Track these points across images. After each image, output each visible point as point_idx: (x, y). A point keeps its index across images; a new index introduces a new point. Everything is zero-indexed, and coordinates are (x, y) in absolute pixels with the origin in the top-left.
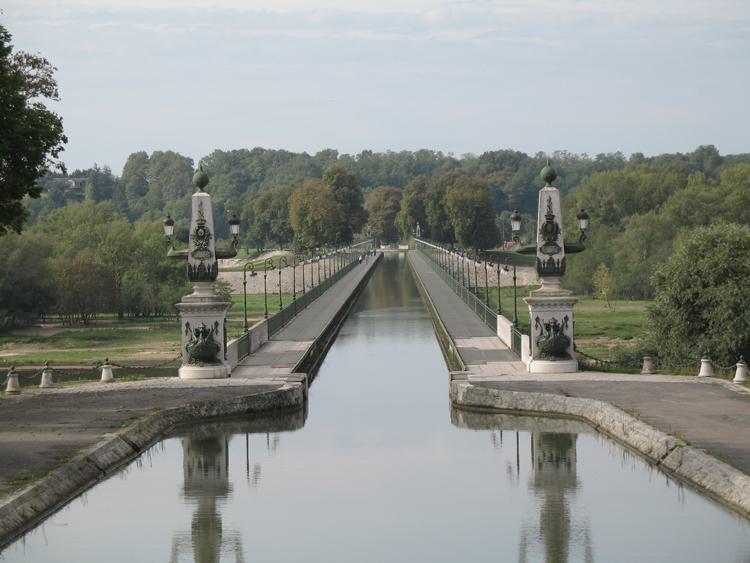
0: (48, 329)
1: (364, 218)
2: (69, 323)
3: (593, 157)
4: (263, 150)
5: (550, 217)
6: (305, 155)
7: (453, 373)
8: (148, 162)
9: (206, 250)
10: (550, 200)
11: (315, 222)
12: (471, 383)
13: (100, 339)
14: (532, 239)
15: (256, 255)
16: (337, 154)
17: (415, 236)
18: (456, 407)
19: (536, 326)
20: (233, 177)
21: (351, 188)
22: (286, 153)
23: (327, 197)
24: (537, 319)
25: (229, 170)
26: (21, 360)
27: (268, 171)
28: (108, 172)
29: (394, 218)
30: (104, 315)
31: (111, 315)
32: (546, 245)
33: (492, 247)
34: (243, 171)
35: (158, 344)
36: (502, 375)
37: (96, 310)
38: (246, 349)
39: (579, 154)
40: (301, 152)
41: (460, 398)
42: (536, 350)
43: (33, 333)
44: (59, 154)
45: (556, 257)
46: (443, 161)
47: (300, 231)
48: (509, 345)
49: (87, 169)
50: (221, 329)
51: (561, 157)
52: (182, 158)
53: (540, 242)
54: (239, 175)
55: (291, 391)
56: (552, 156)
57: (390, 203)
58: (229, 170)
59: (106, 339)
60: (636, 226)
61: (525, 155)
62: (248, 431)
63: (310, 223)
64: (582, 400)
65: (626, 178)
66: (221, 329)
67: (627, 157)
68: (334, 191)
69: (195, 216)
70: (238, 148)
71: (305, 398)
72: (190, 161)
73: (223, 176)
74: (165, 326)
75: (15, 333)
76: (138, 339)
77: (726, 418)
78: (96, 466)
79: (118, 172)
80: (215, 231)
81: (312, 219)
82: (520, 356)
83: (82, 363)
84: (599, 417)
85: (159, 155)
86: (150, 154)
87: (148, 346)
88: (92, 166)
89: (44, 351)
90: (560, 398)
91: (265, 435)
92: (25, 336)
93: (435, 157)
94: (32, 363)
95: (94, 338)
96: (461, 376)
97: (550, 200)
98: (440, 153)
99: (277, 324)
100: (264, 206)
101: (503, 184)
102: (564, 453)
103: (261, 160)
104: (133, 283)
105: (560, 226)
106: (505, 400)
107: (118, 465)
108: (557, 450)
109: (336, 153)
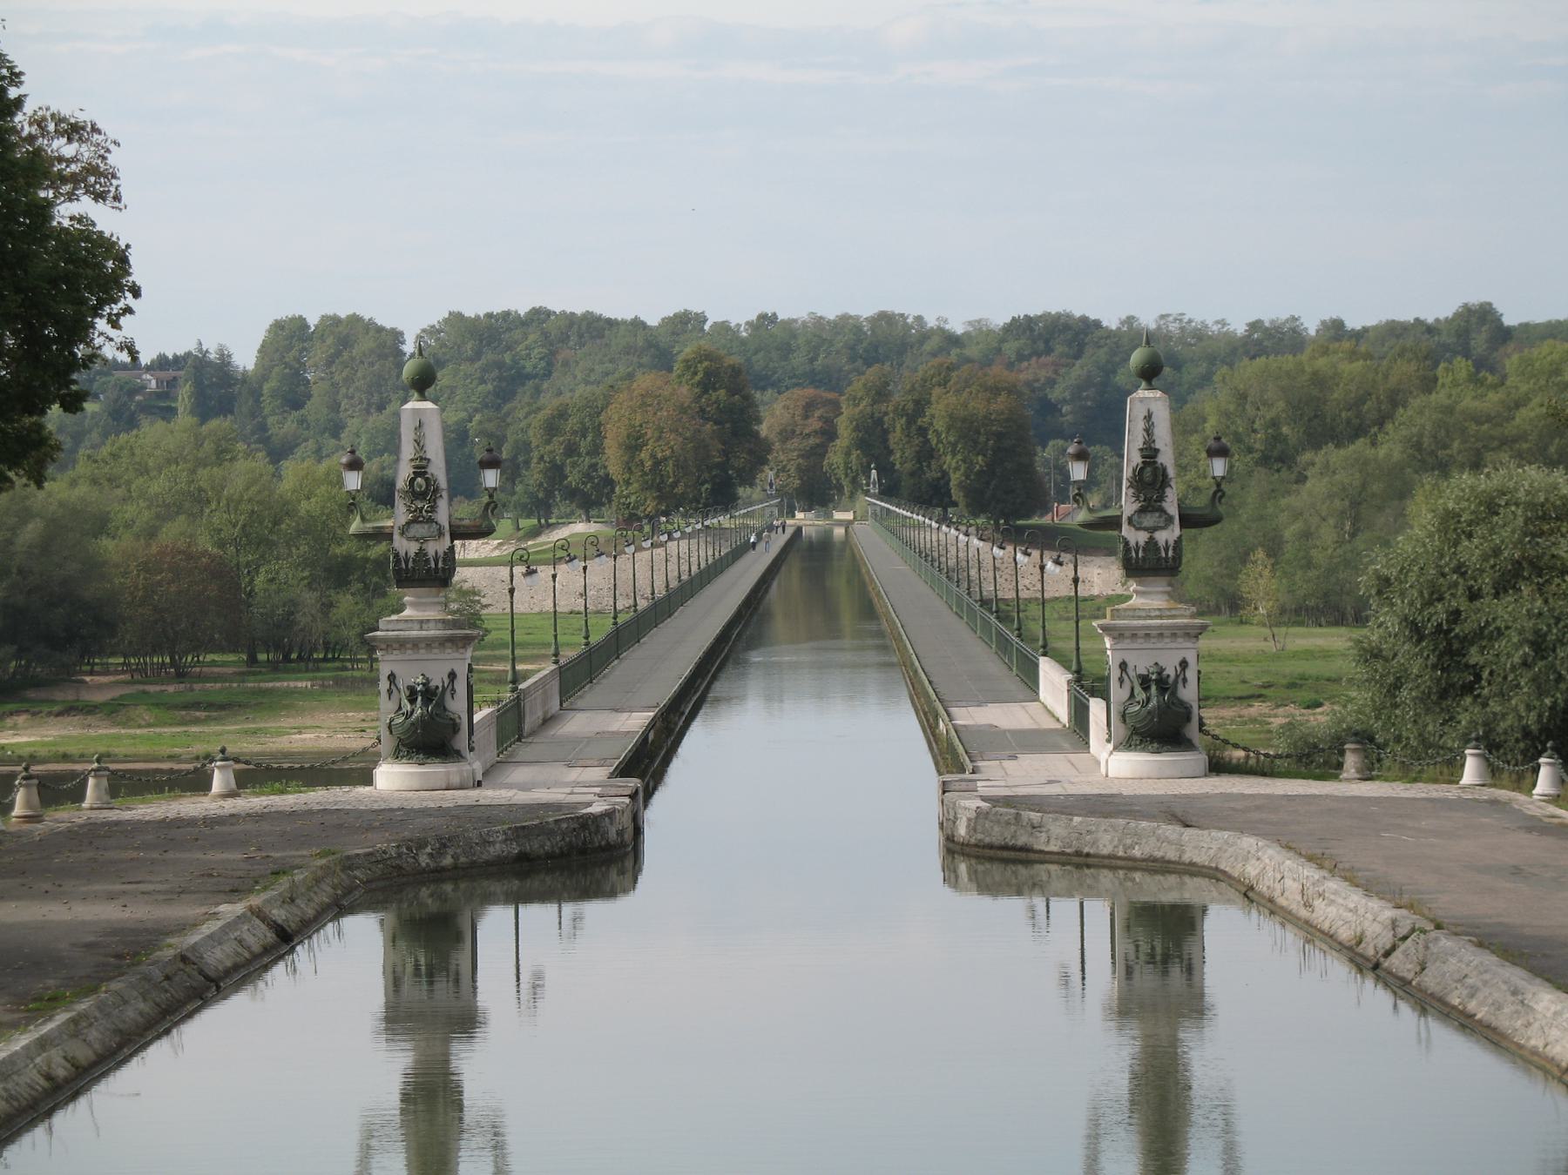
0: (101, 685)
1: (760, 454)
2: (143, 674)
3: (1239, 327)
4: (549, 313)
5: (1150, 453)
6: (637, 324)
7: (948, 777)
8: (310, 338)
9: (430, 521)
10: (1148, 417)
11: (657, 463)
12: (984, 799)
13: (210, 706)
14: (1112, 499)
15: (535, 533)
16: (705, 320)
17: (867, 493)
18: (953, 848)
19: (1121, 680)
20: (484, 370)
21: (732, 392)
22: (599, 318)
23: (683, 410)
24: (1123, 666)
25: (478, 355)
26: (43, 752)
27: (560, 357)
28: (225, 360)
29: (823, 456)
30: (216, 657)
31: (232, 657)
32: (1142, 511)
33: (1028, 517)
34: (507, 358)
35: (330, 719)
36: (1050, 782)
37: (200, 646)
38: (514, 727)
39: (1210, 322)
40: (629, 317)
41: (962, 831)
42: (1120, 730)
43: (66, 695)
44: (123, 321)
45: (1162, 537)
46: (926, 335)
47: (628, 483)
48: (1065, 719)
49: (180, 352)
50: (461, 687)
51: (1174, 327)
52: (380, 329)
53: (1128, 504)
54: (500, 365)
55: (609, 814)
56: (1153, 326)
57: (814, 424)
58: (478, 355)
59: (222, 707)
60: (1328, 472)
61: (1097, 324)
62: (517, 899)
63: (648, 464)
64: (1214, 833)
65: (1308, 369)
66: (461, 687)
67: (1311, 326)
68: (698, 398)
69: (408, 451)
70: (497, 310)
71: (638, 831)
72: (397, 336)
73: (465, 367)
74: (345, 679)
75: (31, 694)
76: (286, 707)
77: (1516, 871)
78: (201, 972)
79: (245, 359)
80: (449, 481)
81: (653, 456)
82: (1087, 743)
83: (171, 758)
84: (1252, 870)
85: (331, 323)
86: (313, 321)
87: (309, 722)
88: (191, 347)
89: (92, 732)
90: (1171, 831)
91: (555, 907)
92: (53, 702)
93: (908, 327)
94: (66, 757)
95: (196, 705)
96: (964, 785)
97: (1148, 417)
98: (919, 319)
99: (580, 675)
100: (551, 429)
101: (1051, 383)
102: (1179, 946)
103: (545, 335)
104: (279, 591)
105: (1171, 472)
106: (1055, 835)
107: (247, 970)
108: (1163, 939)
109: (701, 318)
